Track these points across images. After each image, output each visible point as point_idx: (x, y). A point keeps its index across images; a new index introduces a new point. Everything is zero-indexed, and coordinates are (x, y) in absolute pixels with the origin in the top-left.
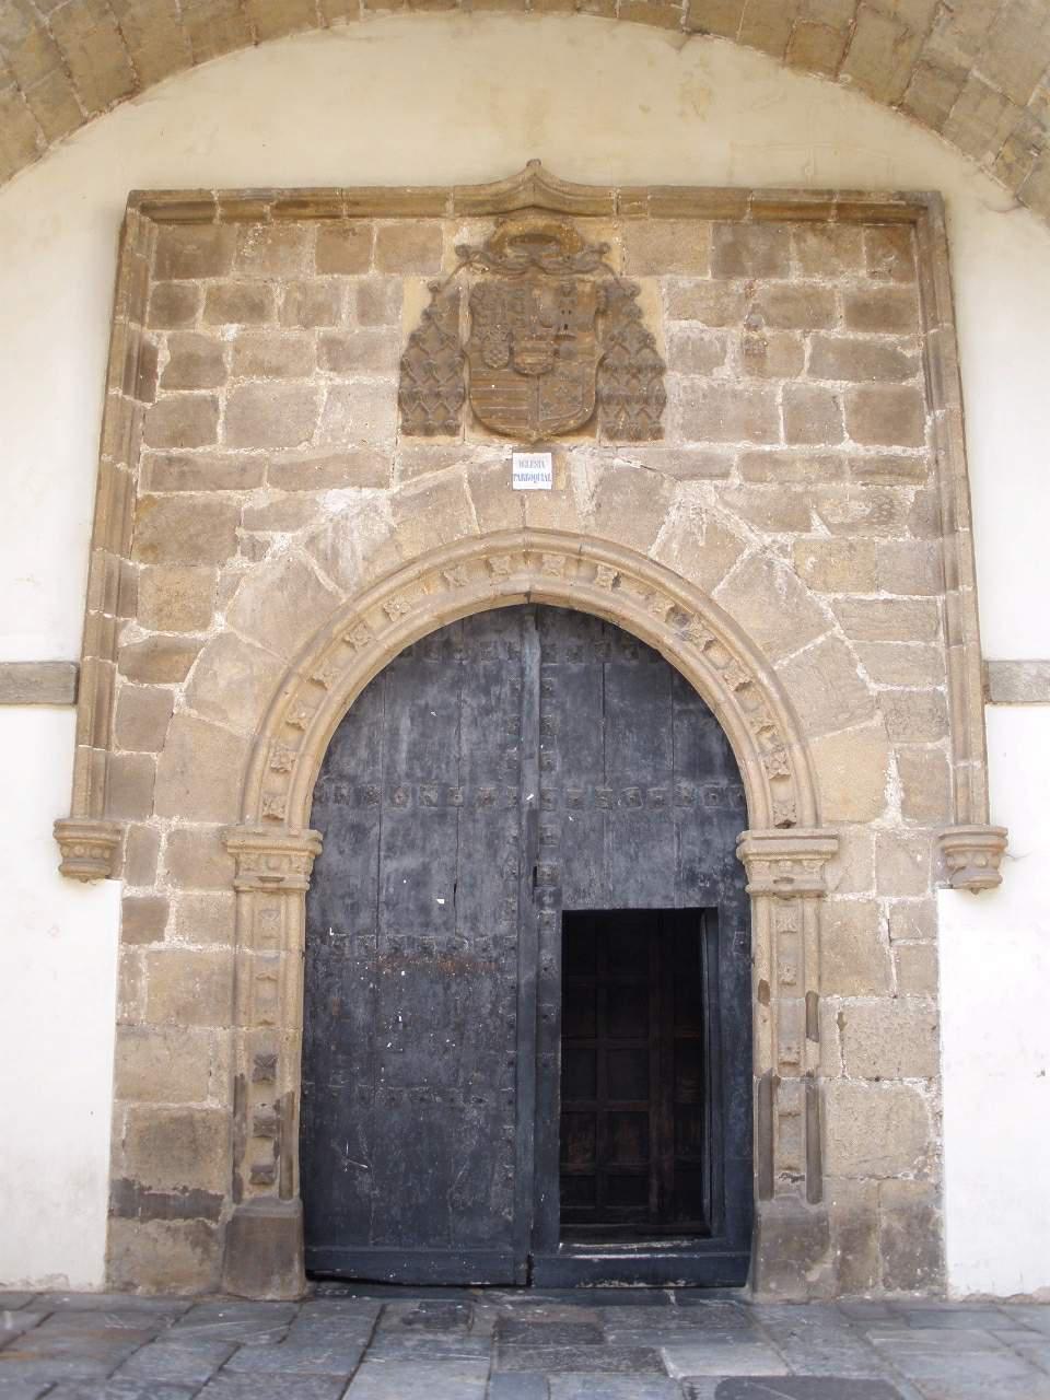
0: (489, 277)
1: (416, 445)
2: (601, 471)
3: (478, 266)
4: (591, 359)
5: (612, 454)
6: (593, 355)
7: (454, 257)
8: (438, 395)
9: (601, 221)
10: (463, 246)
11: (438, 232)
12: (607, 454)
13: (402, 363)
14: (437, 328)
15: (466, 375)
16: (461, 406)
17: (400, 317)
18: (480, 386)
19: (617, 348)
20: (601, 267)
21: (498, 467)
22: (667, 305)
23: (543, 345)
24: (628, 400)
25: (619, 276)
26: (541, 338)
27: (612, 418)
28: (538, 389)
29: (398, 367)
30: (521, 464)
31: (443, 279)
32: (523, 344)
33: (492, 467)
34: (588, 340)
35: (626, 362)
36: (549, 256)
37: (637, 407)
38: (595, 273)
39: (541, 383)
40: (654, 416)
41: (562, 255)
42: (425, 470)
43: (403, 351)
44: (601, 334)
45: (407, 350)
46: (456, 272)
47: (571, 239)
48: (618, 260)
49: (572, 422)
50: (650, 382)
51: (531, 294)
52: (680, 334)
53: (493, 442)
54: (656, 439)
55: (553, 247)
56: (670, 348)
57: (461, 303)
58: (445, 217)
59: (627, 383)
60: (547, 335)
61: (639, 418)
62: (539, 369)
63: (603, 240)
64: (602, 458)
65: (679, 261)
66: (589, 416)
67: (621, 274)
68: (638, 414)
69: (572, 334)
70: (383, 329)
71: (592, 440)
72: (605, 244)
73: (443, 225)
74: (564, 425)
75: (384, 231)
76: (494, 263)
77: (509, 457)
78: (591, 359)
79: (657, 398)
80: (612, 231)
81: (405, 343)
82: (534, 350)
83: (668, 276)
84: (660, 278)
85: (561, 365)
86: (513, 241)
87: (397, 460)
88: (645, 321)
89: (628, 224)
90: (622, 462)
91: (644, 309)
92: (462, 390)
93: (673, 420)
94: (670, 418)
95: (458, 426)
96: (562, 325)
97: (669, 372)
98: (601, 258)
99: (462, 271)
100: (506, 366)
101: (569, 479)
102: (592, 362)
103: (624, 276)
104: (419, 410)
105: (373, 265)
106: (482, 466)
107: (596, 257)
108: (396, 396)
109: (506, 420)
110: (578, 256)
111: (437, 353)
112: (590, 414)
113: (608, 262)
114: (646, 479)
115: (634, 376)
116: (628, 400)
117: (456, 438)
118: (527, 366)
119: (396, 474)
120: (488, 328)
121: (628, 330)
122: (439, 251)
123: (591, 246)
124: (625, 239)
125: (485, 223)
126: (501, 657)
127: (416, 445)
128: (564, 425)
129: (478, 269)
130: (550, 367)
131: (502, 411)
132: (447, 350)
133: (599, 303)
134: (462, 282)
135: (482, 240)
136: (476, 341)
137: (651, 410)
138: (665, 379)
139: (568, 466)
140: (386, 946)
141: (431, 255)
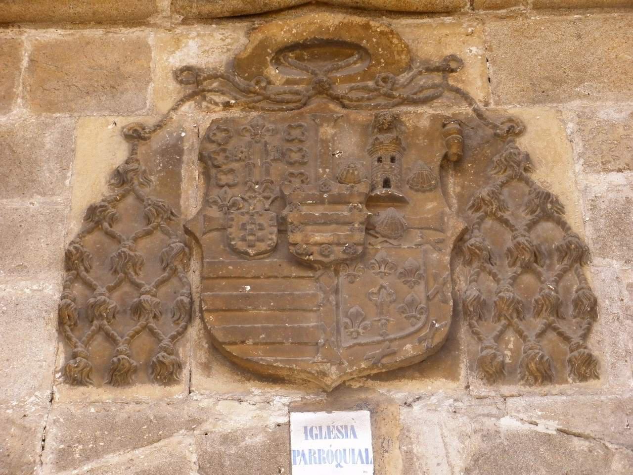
0: (236, 113)
1: (93, 403)
2: (475, 443)
3: (219, 99)
4: (440, 236)
5: (494, 411)
6: (442, 231)
7: (173, 85)
8: (138, 310)
9: (443, 24)
10: (188, 69)
11: (142, 48)
12: (480, 410)
13: (68, 256)
14: (139, 198)
15: (194, 278)
16: (185, 328)
17: (67, 182)
18: (222, 289)
19: (489, 223)
20: (446, 94)
21: (259, 439)
22: (579, 149)
23: (344, 211)
24: (518, 309)
25: (481, 106)
26: (337, 200)
27: (489, 341)
28: (336, 291)
29: (61, 265)
30: (308, 431)
31: (151, 121)
32: (305, 210)
33: (248, 441)
34: (430, 206)
35: (510, 244)
36: (349, 79)
37: (539, 323)
38: (436, 103)
39: (342, 279)
40: (576, 339)
41: (372, 77)
42: (107, 450)
43: (71, 238)
44: (455, 201)
45: (78, 236)
46: (174, 109)
47: (389, 48)
48: (479, 83)
49: (408, 346)
50: (560, 277)
51: (317, 131)
52: (611, 195)
53: (250, 393)
54: (583, 378)
55: (358, 66)
56: (593, 220)
57: (185, 158)
58: (155, 25)
59: (515, 279)
60: (351, 195)
61: (544, 342)
62: (338, 253)
63: (448, 52)
64: (474, 418)
65: (593, 77)
66: (438, 339)
67: (487, 104)
68: (541, 335)
69: (397, 193)
70: (35, 203)
71: (451, 385)
72: (453, 58)
73: (151, 36)
74: (394, 353)
75: (39, 48)
76: (247, 92)
77: (283, 420)
78: (440, 236)
79: (577, 303)
80: (464, 38)
81: (75, 226)
82: (326, 221)
83: (576, 103)
84: (561, 106)
85: (380, 250)
86: (283, 52)
87: (53, 431)
88: (539, 177)
89: (492, 26)
90: (519, 424)
91: (534, 157)
92: (186, 300)
93: (614, 344)
94: (608, 340)
95: (179, 366)
96: (380, 180)
97: (597, 260)
98: (445, 78)
99: (187, 107)
100: (274, 249)
101: (409, 458)
102: (442, 241)
103: (492, 106)
104: (99, 339)
105: (19, 101)
106: (226, 439)
107: (437, 78)
108: (54, 316)
109: (273, 345)
110: (403, 78)
111: (135, 239)
112: (445, 330)
113: (460, 86)
114: (570, 454)
115: (527, 268)
116: (518, 309)
117: (175, 388)
118: (315, 249)
119: (49, 457)
120: (236, 190)
121: (506, 191)
122: (144, 78)
123: (427, 61)
124: (489, 49)
125: (228, 33)
126: (435, 401)
127: (93, 403)
128: (394, 353)
129: (216, 104)
130: (360, 249)
131: (265, 329)
132: (158, 234)
133: (448, 146)
134: (186, 125)
135: (224, 58)
136: (214, 212)
137: (571, 327)
138: (589, 272)
139: (405, 433)
140: (409, 297)
141: (129, 84)
